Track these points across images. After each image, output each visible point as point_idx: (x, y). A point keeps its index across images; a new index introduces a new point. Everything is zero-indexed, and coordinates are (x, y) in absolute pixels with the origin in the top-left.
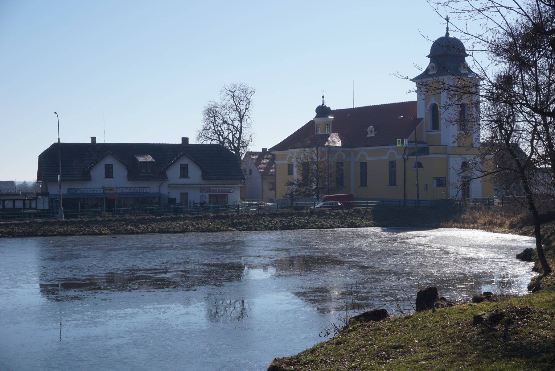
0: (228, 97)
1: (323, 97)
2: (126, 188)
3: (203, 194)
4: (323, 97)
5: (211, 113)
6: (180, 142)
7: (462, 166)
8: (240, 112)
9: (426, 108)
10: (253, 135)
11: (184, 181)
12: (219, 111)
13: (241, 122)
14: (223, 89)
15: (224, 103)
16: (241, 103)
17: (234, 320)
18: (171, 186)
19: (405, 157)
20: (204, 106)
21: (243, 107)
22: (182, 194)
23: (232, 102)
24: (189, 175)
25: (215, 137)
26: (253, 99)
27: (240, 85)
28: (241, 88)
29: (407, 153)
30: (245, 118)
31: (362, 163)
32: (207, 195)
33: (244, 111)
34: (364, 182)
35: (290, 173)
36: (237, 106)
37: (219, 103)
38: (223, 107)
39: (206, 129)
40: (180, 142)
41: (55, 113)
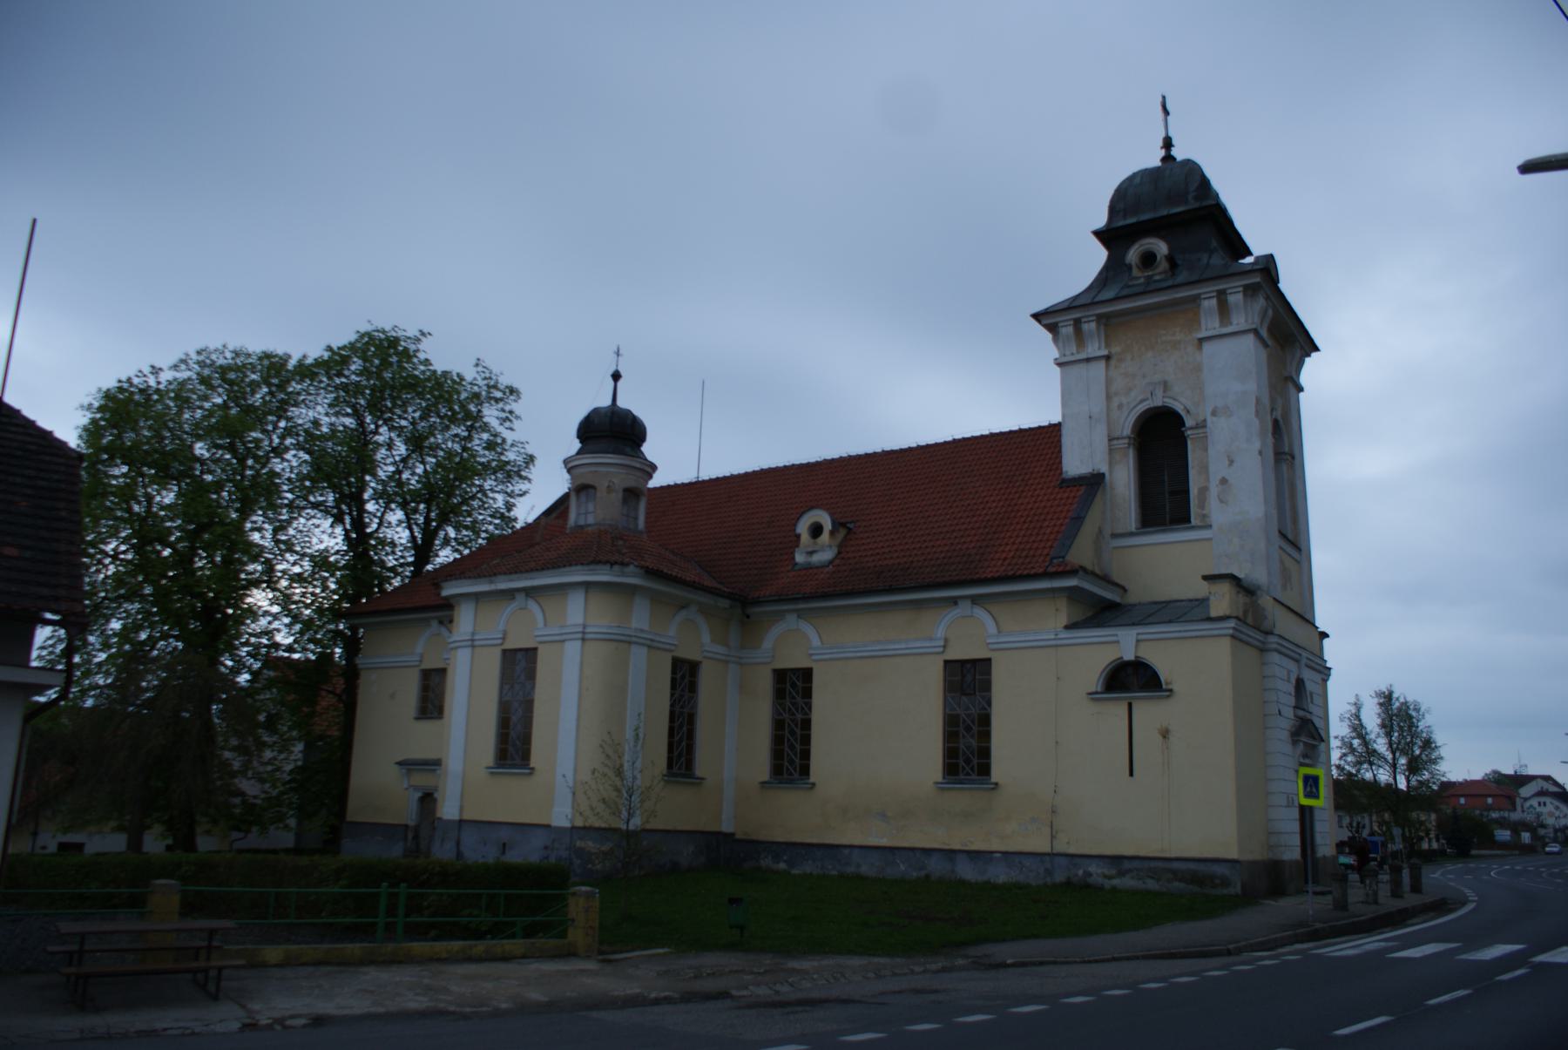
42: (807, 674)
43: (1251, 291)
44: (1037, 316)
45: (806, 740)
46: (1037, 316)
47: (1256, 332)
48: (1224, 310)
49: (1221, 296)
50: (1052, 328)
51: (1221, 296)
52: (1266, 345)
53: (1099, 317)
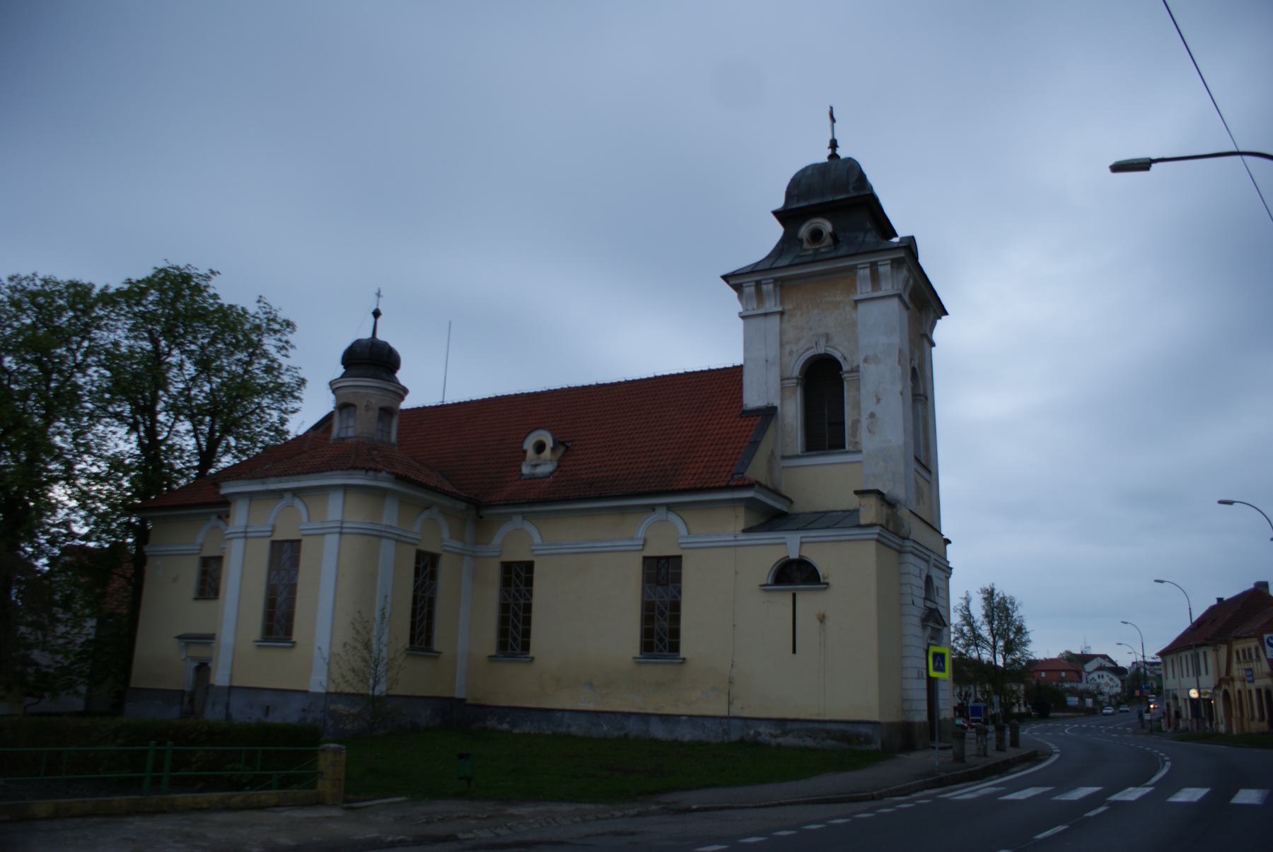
42: (529, 566)
43: (897, 264)
44: (725, 278)
45: (527, 621)
46: (725, 278)
47: (900, 296)
48: (875, 278)
49: (874, 267)
50: (738, 288)
51: (874, 267)
52: (908, 308)
53: (776, 280)
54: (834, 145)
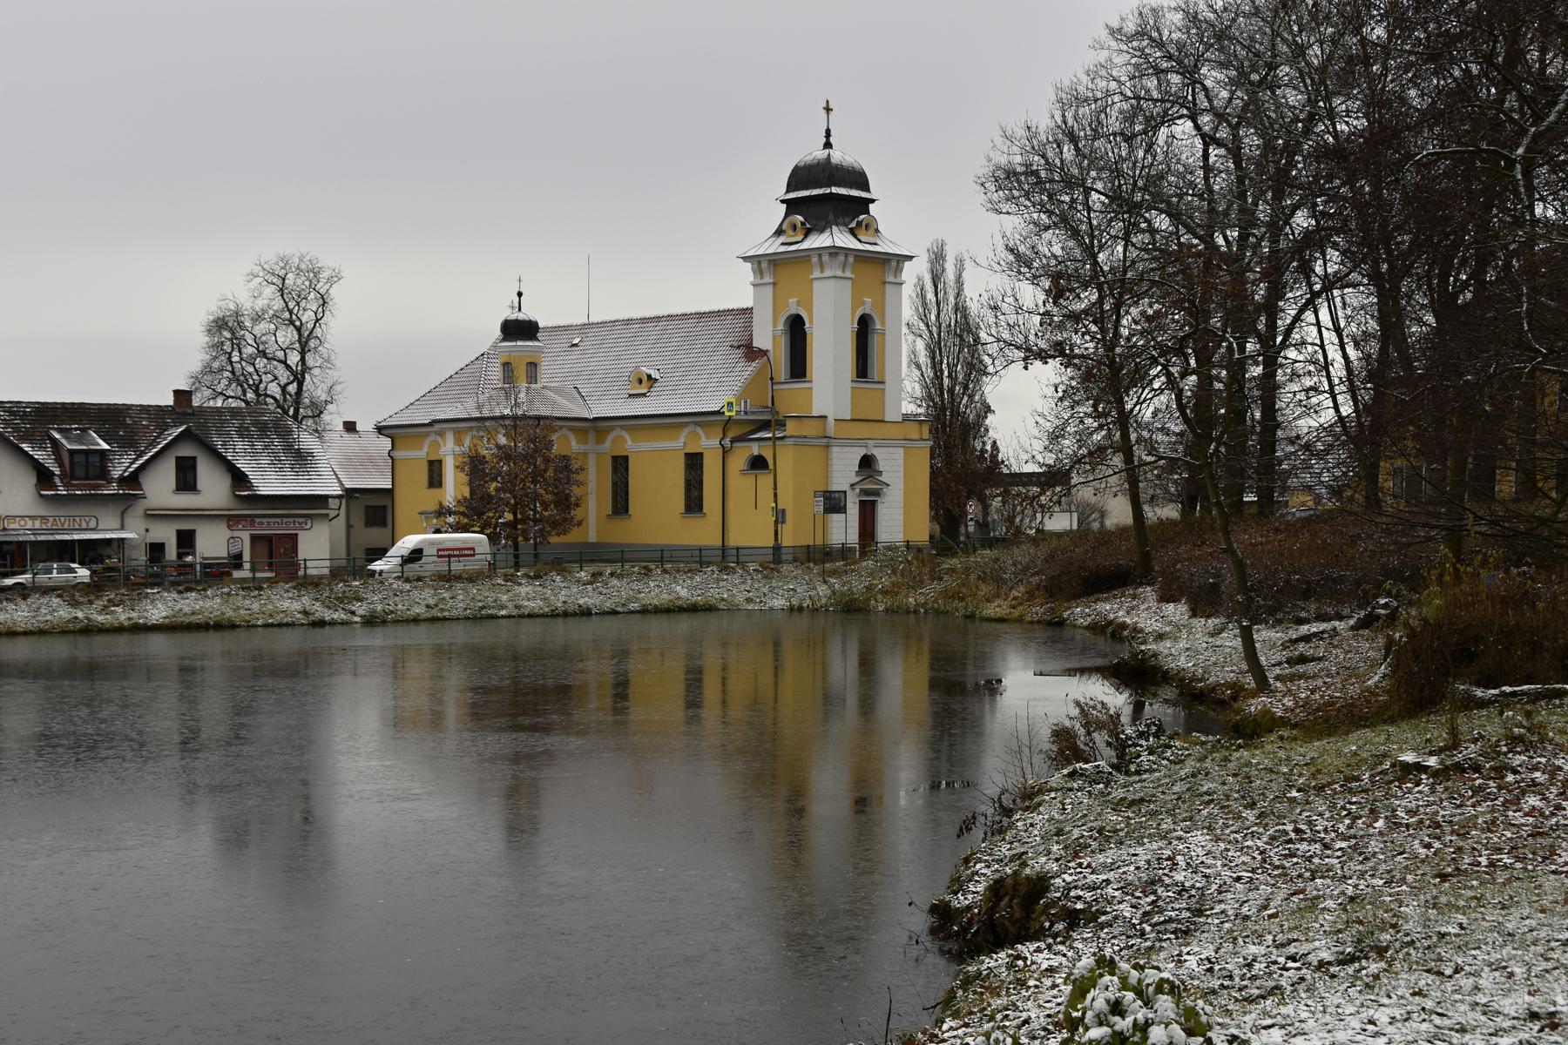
0: (270, 291)
1: (520, 294)
2: (33, 518)
3: (236, 534)
4: (520, 294)
5: (226, 328)
6: (169, 400)
7: (860, 466)
8: (299, 330)
9: (775, 324)
10: (338, 388)
11: (185, 500)
12: (248, 324)
13: (303, 353)
14: (257, 269)
15: (260, 304)
16: (303, 304)
17: (281, 824)
18: (154, 516)
19: (727, 442)
20: (207, 308)
21: (307, 317)
22: (179, 533)
23: (278, 304)
24: (199, 487)
25: (234, 390)
26: (336, 293)
27: (301, 261)
28: (303, 266)
29: (731, 435)
30: (312, 344)
31: (431, 463)
32: (246, 536)
33: (310, 326)
34: (621, 503)
35: (435, 480)
36: (291, 312)
37: (248, 305)
38: (257, 318)
39: (208, 370)
40: (169, 400)
41: (828, 110)
54: (828, 133)
